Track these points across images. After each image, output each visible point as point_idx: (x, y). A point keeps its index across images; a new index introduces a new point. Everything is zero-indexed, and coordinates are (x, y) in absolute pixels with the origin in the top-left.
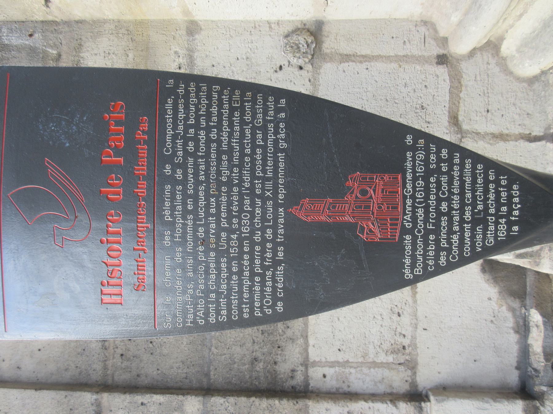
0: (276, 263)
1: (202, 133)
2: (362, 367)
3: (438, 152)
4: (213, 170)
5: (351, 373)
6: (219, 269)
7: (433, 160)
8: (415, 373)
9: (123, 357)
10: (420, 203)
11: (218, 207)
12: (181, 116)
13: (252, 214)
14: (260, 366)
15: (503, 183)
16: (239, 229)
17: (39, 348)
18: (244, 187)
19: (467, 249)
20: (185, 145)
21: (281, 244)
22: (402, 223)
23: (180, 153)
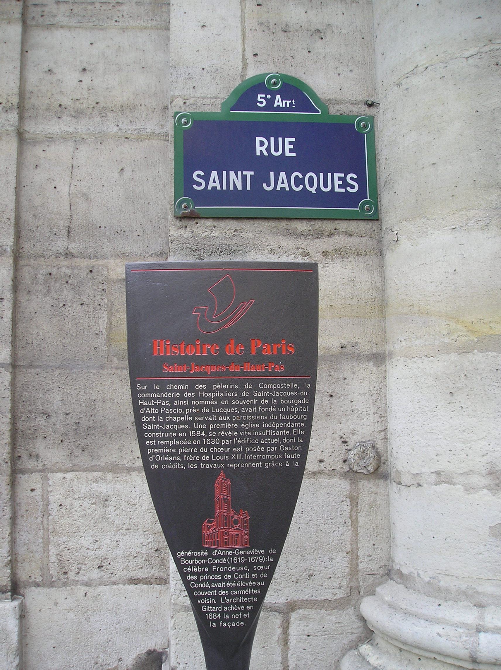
0: (185, 463)
1: (274, 409)
2: (43, 529)
3: (264, 571)
4: (249, 417)
5: (37, 518)
6: (181, 423)
7: (259, 568)
8: (38, 585)
9: (48, 276)
10: (230, 560)
11: (223, 422)
12: (286, 394)
13: (220, 446)
14: (41, 421)
15: (245, 616)
16: (208, 437)
17: (57, 188)
18: (238, 439)
19: (199, 593)
20: (266, 398)
21: (199, 466)
22: (216, 549)
23: (260, 394)
